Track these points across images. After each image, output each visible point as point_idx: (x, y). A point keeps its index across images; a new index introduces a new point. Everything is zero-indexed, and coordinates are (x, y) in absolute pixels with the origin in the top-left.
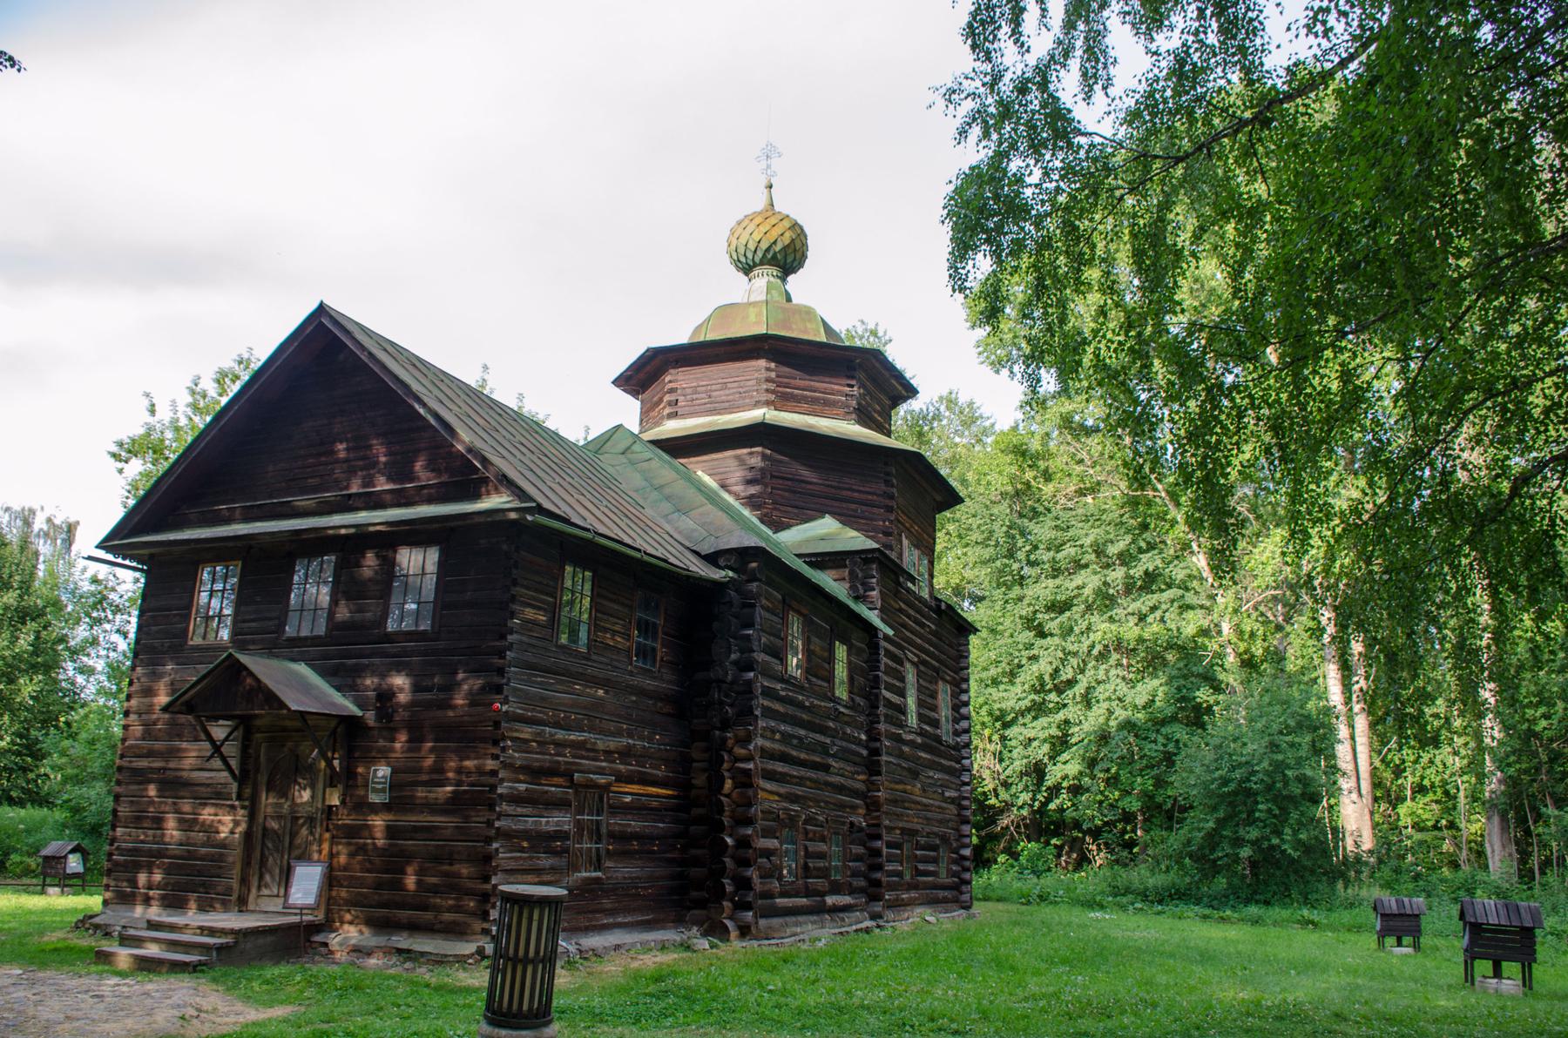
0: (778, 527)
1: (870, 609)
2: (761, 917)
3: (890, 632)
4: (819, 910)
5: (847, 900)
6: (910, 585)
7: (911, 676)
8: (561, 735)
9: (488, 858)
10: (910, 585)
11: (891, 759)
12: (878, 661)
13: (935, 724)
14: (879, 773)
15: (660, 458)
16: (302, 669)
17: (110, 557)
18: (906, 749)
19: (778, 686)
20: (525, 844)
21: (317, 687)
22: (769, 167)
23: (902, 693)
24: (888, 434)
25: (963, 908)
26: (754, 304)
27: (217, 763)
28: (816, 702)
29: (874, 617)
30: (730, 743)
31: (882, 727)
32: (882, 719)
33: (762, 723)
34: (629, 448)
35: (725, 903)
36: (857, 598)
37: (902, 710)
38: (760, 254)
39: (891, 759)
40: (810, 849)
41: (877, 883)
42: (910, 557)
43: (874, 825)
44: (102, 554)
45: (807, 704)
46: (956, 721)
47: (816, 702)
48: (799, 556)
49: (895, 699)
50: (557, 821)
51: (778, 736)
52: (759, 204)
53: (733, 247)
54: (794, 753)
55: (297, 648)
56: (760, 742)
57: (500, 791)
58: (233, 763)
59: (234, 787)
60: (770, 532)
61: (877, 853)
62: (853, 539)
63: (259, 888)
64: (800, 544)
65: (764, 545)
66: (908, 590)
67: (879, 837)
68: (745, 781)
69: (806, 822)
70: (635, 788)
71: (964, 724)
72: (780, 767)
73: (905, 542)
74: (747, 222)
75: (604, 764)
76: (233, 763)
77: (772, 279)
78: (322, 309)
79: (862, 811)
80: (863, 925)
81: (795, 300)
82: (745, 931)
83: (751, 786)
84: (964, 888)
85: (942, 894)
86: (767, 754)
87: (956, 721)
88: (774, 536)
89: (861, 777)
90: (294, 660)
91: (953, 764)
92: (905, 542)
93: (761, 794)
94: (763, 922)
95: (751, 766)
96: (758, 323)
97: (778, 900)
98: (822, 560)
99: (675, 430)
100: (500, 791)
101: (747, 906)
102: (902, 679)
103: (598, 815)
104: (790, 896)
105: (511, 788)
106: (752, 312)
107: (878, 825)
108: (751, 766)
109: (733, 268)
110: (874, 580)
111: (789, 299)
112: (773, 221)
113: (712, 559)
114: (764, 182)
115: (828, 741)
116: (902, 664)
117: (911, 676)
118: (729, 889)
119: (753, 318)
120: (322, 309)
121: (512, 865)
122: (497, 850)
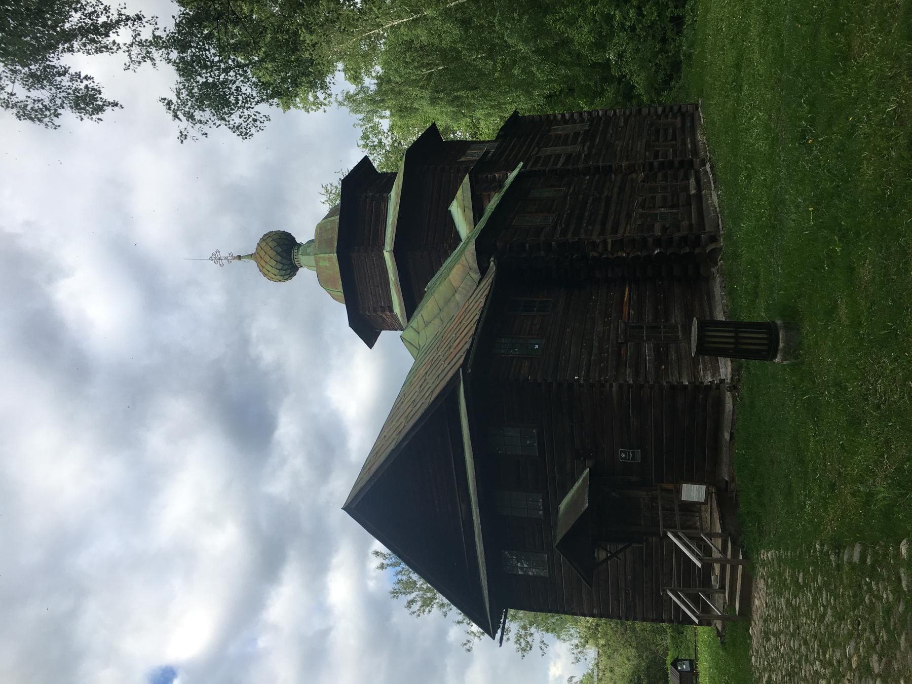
0: (458, 239)
1: (507, 177)
2: (704, 230)
3: (522, 164)
4: (699, 197)
5: (692, 181)
6: (490, 155)
7: (549, 151)
8: (595, 351)
9: (673, 387)
10: (490, 155)
11: (601, 160)
12: (540, 170)
13: (577, 134)
14: (611, 167)
15: (421, 310)
16: (562, 506)
17: (499, 631)
18: (594, 151)
19: (559, 228)
20: (663, 367)
21: (573, 496)
22: (226, 258)
23: (558, 157)
24: (393, 176)
25: (697, 109)
26: (317, 262)
27: (620, 555)
28: (567, 206)
29: (512, 175)
30: (595, 254)
31: (581, 166)
32: (575, 166)
33: (583, 236)
34: (415, 330)
35: (696, 253)
36: (501, 186)
37: (569, 156)
38: (285, 261)
39: (601, 160)
40: (661, 179)
41: (682, 163)
42: (474, 155)
43: (644, 168)
44: (498, 635)
45: (569, 212)
46: (574, 122)
47: (567, 206)
48: (475, 224)
49: (562, 160)
50: (648, 350)
51: (590, 227)
52: (253, 263)
53: (281, 278)
54: (600, 217)
55: (551, 508)
56: (594, 237)
57: (631, 382)
58: (620, 546)
59: (635, 545)
60: (462, 243)
61: (662, 164)
62: (464, 192)
63: (696, 528)
64: (468, 223)
65: (473, 241)
66: (493, 156)
67: (651, 164)
68: (619, 244)
69: (643, 208)
70: (625, 308)
71: (576, 116)
72: (609, 226)
73: (463, 159)
74: (264, 270)
75: (612, 326)
76: (620, 546)
77: (300, 253)
78: (348, 508)
79: (634, 175)
80: (708, 169)
81: (313, 237)
82: (714, 239)
83: (622, 239)
84: (684, 110)
85: (688, 124)
86: (602, 232)
87: (574, 122)
88: (463, 241)
89: (613, 176)
90: (557, 511)
91: (602, 122)
92: (463, 159)
93: (627, 234)
94: (707, 229)
95: (610, 240)
96: (330, 259)
97: (693, 222)
98: (478, 211)
99: (401, 308)
100: (631, 382)
101: (698, 237)
102: (550, 156)
103: (643, 328)
104: (691, 214)
105: (629, 376)
106: (322, 264)
107: (644, 165)
108: (610, 240)
109: (288, 282)
110: (489, 176)
111: (312, 241)
112: (262, 253)
113: (483, 270)
114: (237, 261)
115: (591, 198)
116: (540, 157)
117: (549, 151)
118: (687, 250)
119: (327, 264)
120: (348, 508)
121: (676, 373)
122: (667, 382)
